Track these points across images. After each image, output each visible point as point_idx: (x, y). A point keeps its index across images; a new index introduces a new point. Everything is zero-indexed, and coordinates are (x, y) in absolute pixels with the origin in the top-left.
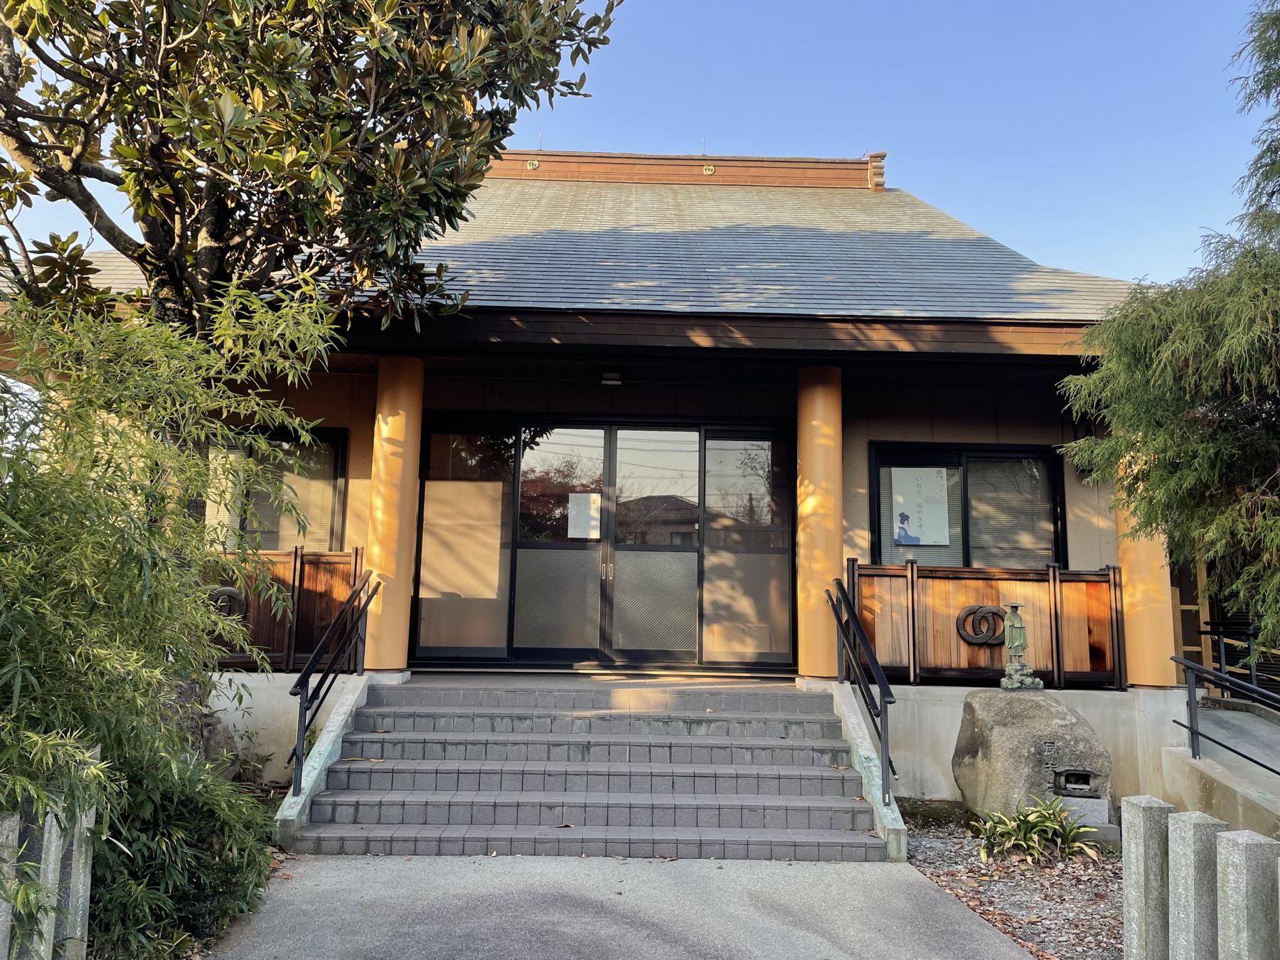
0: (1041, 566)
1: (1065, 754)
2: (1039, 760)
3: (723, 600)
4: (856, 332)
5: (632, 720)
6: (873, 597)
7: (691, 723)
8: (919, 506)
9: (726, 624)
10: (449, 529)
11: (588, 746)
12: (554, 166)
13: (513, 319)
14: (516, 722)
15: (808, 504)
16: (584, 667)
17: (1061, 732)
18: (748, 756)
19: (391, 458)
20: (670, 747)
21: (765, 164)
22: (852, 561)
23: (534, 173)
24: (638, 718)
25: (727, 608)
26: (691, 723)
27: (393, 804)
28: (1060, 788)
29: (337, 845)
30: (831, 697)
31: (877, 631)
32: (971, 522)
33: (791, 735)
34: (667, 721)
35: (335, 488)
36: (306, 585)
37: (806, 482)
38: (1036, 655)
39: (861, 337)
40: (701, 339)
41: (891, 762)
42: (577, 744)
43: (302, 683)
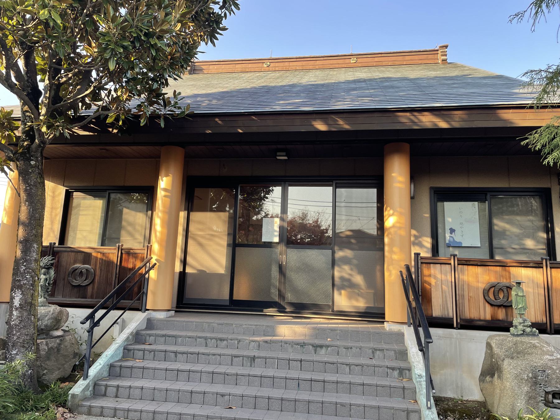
0: (538, 259)
1: (552, 379)
2: (535, 382)
3: (346, 276)
4: (412, 117)
5: (283, 344)
6: (430, 276)
7: (317, 347)
8: (461, 224)
9: (349, 290)
10: (202, 237)
11: (253, 358)
12: (277, 64)
13: (217, 120)
14: (219, 342)
15: (390, 221)
16: (270, 311)
17: (550, 364)
18: (347, 369)
19: (164, 198)
20: (301, 361)
21: (383, 55)
22: (417, 255)
23: (268, 68)
24: (286, 343)
25: (349, 280)
26: (317, 347)
27: (137, 388)
28: (548, 402)
29: (99, 410)
30: (403, 335)
31: (433, 296)
32: (493, 231)
33: (376, 357)
34: (303, 345)
35: (147, 215)
36: (123, 264)
37: (388, 209)
38: (535, 312)
39: (416, 121)
40: (321, 127)
41: (431, 381)
42: (248, 357)
43: (91, 317)
